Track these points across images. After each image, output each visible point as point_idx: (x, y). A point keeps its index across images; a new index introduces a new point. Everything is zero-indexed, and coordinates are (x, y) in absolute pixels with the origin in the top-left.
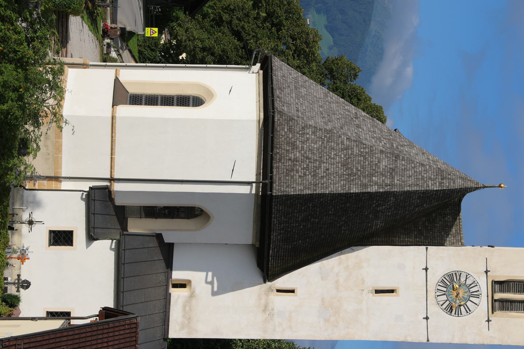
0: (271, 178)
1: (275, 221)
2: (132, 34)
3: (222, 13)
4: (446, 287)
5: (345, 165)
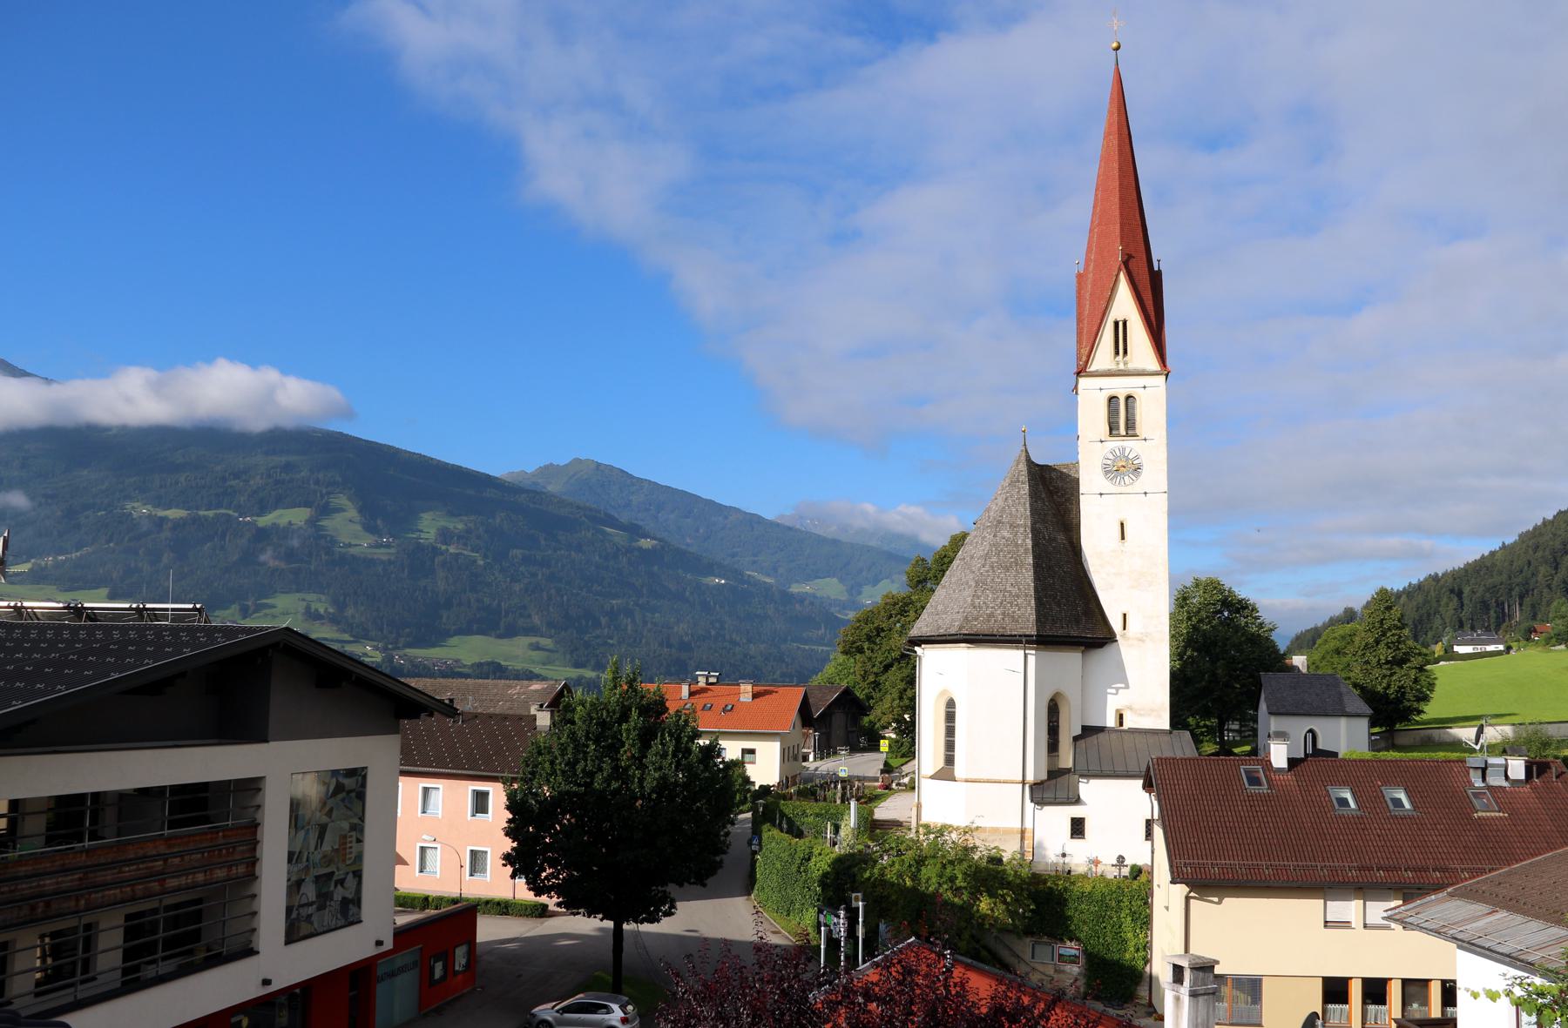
0: (1020, 636)
1: (1060, 633)
2: (886, 764)
3: (867, 682)
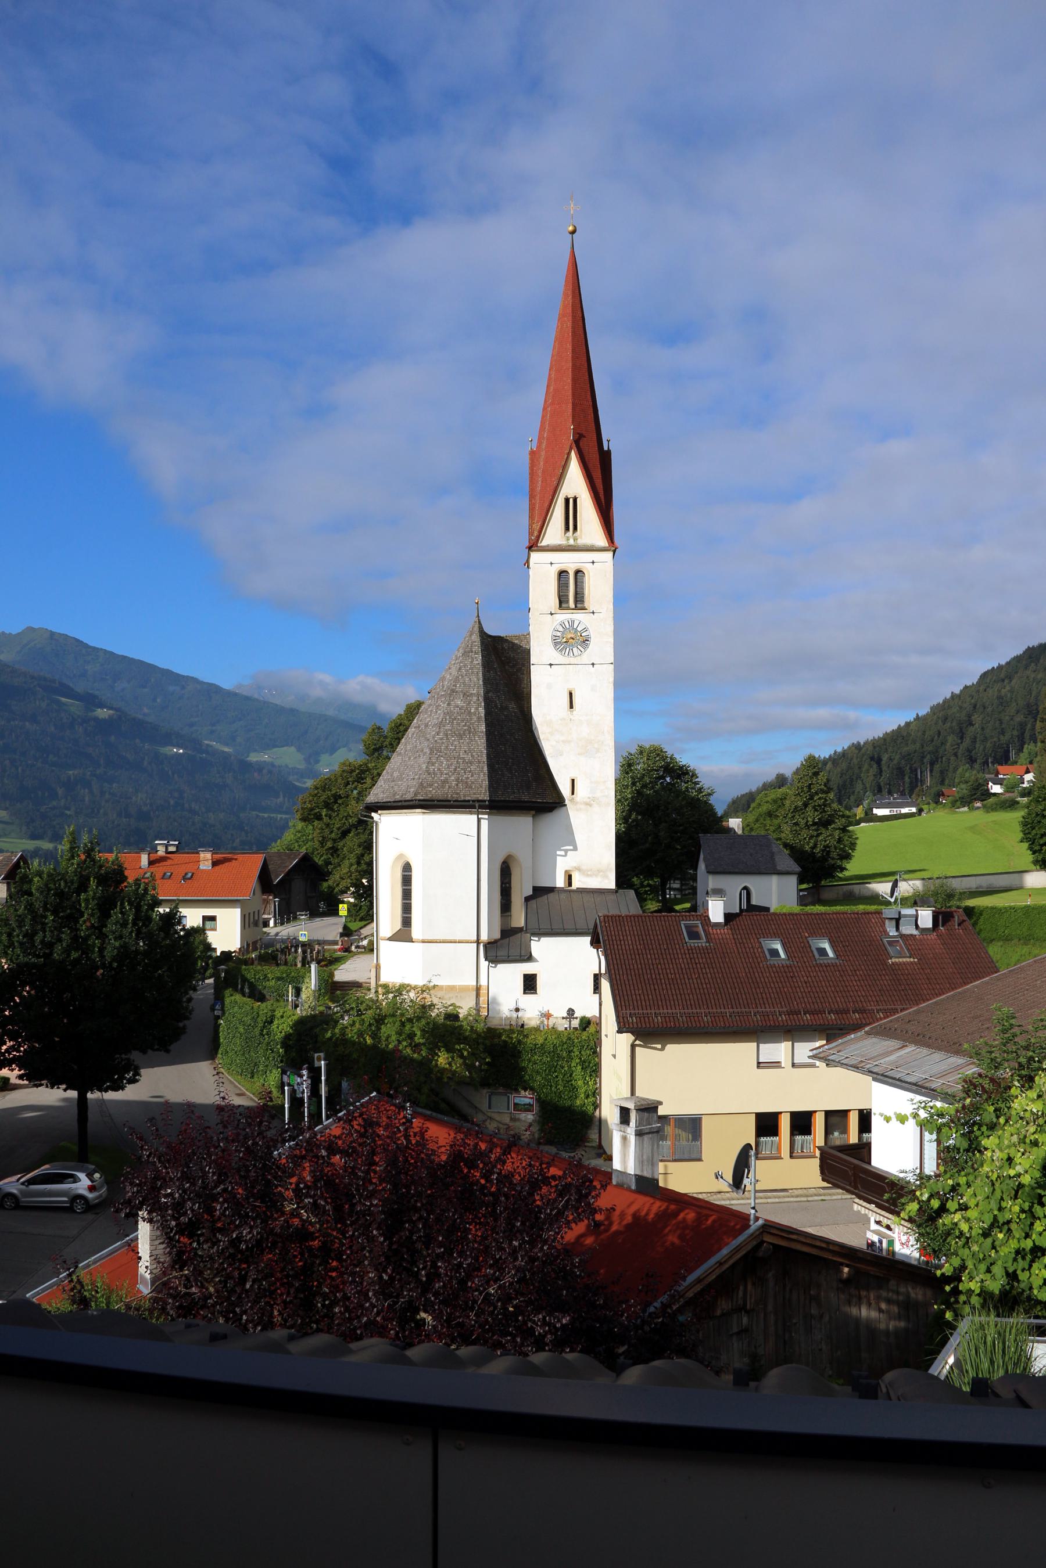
0: (473, 801)
1: (512, 798)
2: (345, 928)
5: (461, 736)
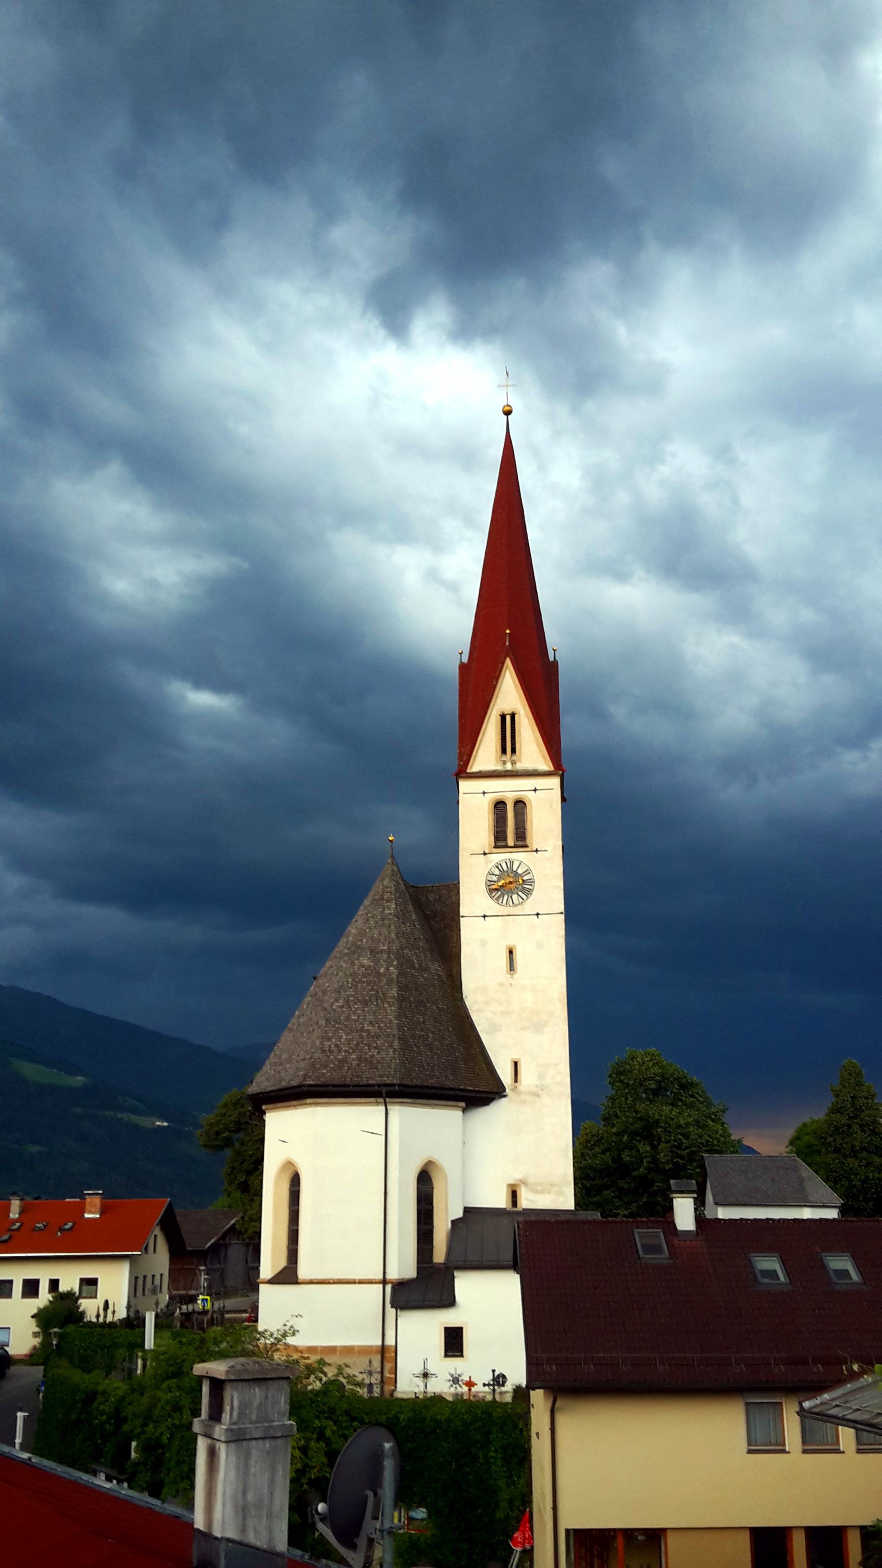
0: (379, 1085)
4: (504, 896)
5: (366, 1003)
